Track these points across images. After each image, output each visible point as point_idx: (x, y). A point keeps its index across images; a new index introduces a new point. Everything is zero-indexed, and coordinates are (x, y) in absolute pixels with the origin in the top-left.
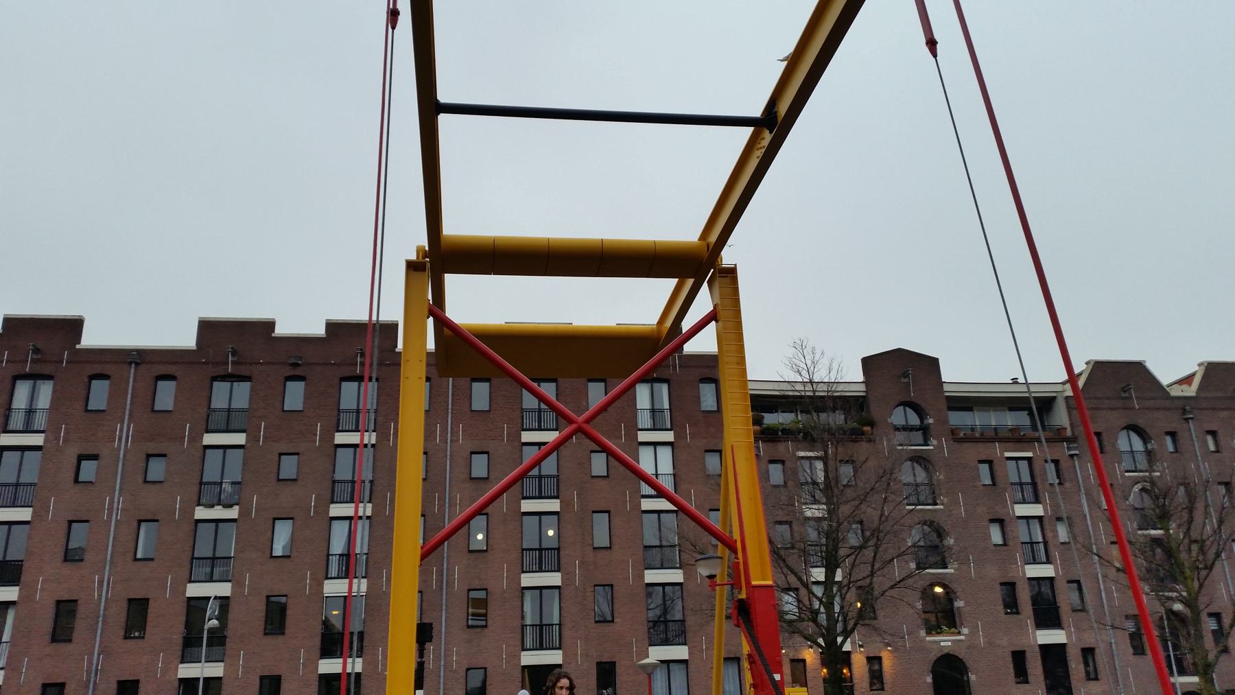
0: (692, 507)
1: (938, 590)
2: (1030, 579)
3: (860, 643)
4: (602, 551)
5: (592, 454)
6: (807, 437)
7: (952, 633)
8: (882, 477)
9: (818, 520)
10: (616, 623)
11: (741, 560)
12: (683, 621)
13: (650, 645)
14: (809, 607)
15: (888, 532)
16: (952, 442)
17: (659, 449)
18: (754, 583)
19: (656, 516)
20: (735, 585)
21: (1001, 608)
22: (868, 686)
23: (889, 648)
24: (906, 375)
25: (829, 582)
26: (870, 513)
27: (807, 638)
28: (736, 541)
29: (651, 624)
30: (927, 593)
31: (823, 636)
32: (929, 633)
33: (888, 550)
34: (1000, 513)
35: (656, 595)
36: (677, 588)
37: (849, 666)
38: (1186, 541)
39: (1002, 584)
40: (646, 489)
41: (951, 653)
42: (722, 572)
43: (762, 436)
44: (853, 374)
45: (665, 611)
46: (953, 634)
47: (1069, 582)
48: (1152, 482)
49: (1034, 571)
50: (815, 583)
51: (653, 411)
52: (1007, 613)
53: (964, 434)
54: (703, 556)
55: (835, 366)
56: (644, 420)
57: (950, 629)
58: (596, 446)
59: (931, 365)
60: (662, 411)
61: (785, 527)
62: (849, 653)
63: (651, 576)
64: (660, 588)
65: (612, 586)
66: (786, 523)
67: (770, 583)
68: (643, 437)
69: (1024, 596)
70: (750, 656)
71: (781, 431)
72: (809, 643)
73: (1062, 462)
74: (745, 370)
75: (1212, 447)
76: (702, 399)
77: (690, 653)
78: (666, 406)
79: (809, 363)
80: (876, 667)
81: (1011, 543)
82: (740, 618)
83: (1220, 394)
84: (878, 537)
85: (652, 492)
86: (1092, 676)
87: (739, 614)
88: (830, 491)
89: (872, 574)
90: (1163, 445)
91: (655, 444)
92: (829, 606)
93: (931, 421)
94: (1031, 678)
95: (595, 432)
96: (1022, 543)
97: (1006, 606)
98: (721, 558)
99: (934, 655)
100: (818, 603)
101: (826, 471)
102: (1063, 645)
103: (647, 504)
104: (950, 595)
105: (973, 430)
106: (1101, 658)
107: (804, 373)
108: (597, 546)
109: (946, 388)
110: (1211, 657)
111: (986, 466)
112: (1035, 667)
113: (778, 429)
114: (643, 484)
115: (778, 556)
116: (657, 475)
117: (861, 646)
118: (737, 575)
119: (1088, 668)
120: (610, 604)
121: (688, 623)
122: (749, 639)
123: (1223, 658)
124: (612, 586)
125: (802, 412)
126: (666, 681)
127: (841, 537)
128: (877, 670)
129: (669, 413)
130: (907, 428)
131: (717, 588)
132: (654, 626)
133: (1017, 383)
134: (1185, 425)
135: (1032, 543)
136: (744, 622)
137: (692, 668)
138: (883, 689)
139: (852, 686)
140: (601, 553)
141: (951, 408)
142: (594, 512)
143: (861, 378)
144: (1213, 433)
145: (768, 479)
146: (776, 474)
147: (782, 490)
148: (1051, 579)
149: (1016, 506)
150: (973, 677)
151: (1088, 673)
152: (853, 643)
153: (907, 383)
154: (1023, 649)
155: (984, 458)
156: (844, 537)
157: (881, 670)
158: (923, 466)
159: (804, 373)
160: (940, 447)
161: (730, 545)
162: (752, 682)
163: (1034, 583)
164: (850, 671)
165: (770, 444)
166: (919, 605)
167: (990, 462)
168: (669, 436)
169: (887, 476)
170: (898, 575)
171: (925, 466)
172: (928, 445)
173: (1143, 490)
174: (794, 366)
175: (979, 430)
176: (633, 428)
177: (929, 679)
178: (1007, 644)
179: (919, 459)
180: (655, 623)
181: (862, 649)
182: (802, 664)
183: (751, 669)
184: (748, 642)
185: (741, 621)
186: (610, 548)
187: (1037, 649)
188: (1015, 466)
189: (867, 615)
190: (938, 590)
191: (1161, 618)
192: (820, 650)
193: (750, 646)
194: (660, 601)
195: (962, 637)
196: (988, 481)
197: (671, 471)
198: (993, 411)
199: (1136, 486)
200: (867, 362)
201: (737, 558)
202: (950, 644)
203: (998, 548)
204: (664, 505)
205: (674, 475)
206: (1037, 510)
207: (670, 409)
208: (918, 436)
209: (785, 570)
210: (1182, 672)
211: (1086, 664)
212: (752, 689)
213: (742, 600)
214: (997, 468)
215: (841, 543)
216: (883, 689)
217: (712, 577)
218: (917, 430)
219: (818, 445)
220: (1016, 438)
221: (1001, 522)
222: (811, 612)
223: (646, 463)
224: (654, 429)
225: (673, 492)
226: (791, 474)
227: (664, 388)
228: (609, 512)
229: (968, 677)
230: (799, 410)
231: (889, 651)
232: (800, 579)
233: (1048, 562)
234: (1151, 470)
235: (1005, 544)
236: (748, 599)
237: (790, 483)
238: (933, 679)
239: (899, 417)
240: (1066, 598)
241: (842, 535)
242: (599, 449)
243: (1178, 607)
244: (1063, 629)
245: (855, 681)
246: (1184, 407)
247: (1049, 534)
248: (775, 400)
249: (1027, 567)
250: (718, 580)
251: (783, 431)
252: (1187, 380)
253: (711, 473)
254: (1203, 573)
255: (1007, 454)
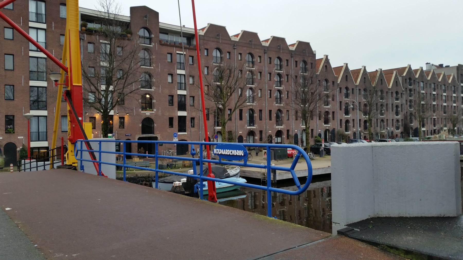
0: (53, 56)
1: (148, 96)
2: (178, 95)
3: (117, 112)
4: (10, 71)
5: (5, 28)
6: (105, 35)
7: (150, 110)
8: (132, 53)
9: (106, 67)
10: (15, 100)
11: (69, 76)
12: (46, 102)
13: (30, 110)
14: (98, 97)
15: (131, 73)
16: (159, 45)
17: (39, 31)
18: (74, 84)
19: (36, 59)
20: (66, 84)
21: (168, 103)
22: (119, 127)
23: (128, 115)
24: (146, 17)
25: (107, 91)
26: (126, 66)
27: (96, 109)
28: (68, 68)
29: (32, 102)
30: (144, 97)
31: (103, 109)
32: (142, 110)
33: (130, 80)
34: (172, 72)
35: (35, 92)
36: (45, 89)
37: (112, 120)
38: (226, 86)
39: (169, 96)
40: (32, 47)
41: (149, 117)
42: (62, 79)
43: (86, 32)
44: (125, 13)
45: (38, 97)
46: (151, 111)
47: (190, 97)
48: (220, 67)
49: (180, 92)
50: (102, 90)
51: (37, 14)
52: (169, 105)
53: (164, 43)
54: (53, 73)
55: (118, 7)
56: (32, 17)
57: (150, 109)
58: (9, 25)
59: (156, 14)
60: (42, 14)
61: (93, 69)
62: (112, 116)
63: (32, 83)
64: (36, 88)
65: (13, 86)
66: (93, 67)
67: (81, 85)
68: (31, 24)
69: (176, 100)
70: (70, 111)
71: (94, 31)
72: (98, 111)
73: (194, 57)
74: (78, 4)
75: (240, 59)
76: (61, 12)
77: (48, 113)
78: (43, 12)
79: (108, 4)
80: (122, 121)
81: (174, 82)
82: (67, 97)
83: (245, 42)
84: (127, 74)
85: (35, 48)
86: (193, 126)
87: (66, 95)
88: (111, 56)
89: (123, 88)
90: (226, 56)
91: (37, 29)
92: (106, 98)
93: (153, 36)
94: (174, 126)
95: (4, 15)
96: (178, 83)
97: (169, 103)
98: (61, 74)
99: (143, 118)
100: (102, 96)
101: (110, 49)
102: (185, 116)
103: (31, 54)
104: (151, 99)
105: (167, 41)
106: (196, 121)
107: (106, 8)
108: (7, 69)
109: (160, 24)
110: (226, 121)
111: (170, 55)
112: (176, 123)
113: (93, 30)
114: (30, 44)
115: (85, 75)
116: (37, 42)
117: (118, 113)
118: (67, 81)
119: (192, 124)
120: (13, 93)
121: (48, 102)
122: (70, 104)
123: (229, 121)
124: (13, 86)
125: (104, 24)
126: (37, 126)
127: (114, 74)
128: (122, 122)
129: (45, 16)
130: (144, 38)
131: (59, 85)
132: (33, 103)
133: (184, 27)
134: (233, 50)
135: (181, 83)
136: (68, 98)
137: (48, 119)
138: (124, 128)
139: (113, 127)
140: (8, 73)
141: (160, 33)
142: (5, 54)
143: (129, 15)
144: (241, 54)
145: (87, 49)
146: (91, 48)
147: (92, 54)
148: (185, 95)
149: (178, 70)
150: (155, 125)
151: (192, 125)
152: (115, 112)
153: (146, 20)
154: (172, 117)
155: (191, 55)
156: (114, 74)
157: (124, 122)
158: (147, 51)
159: (106, 8)
160: (155, 46)
161: (65, 70)
162: (70, 120)
163: (180, 96)
164: (112, 122)
165: (89, 35)
166: (140, 101)
167: (171, 54)
168: (44, 26)
169: (134, 53)
170: (134, 88)
171: (148, 51)
172: (151, 45)
173: (217, 70)
174: (102, 4)
175: (169, 42)
176: (27, 20)
177: (141, 125)
178: (168, 115)
179: (146, 49)
180: (34, 102)
181: (118, 115)
182: (94, 119)
183: (70, 116)
184: (69, 106)
185: (67, 98)
186: (13, 70)
187: (177, 117)
188: (27, 164)
189: (121, 102)
190: (148, 96)
191: (215, 110)
192: (102, 114)
193: (70, 107)
194: (36, 94)
195: (154, 112)
196: (170, 60)
197: (44, 41)
198: (175, 36)
199: (216, 68)
200: (133, 10)
201: (68, 75)
202: (149, 114)
203: (169, 83)
204: (42, 55)
205: (46, 43)
206: (183, 72)
207: (45, 14)
208: (148, 41)
209: (90, 83)
210: (218, 126)
211: (191, 123)
212: (70, 123)
213: (68, 91)
214: (173, 55)
215: (113, 76)
216: (124, 128)
217: (56, 81)
218: (147, 38)
219: (109, 39)
220: (179, 46)
221: (172, 75)
222: (99, 99)
223: (32, 34)
224: (37, 22)
225: (45, 49)
226: (97, 50)
227: (43, 4)
228: (13, 55)
229: (154, 125)
230: (102, 24)
231: (128, 115)
232: (95, 87)
233: (185, 90)
234: (221, 63)
235: (172, 83)
236: (70, 90)
237: (96, 52)
238: (142, 125)
239: (142, 32)
240: (189, 102)
241: (114, 73)
242: (11, 27)
243: (221, 106)
244: (186, 111)
245: (114, 125)
246: (234, 44)
247: (187, 81)
248: (94, 18)
249: (178, 91)
250: (59, 82)
251: (95, 31)
252: (237, 36)
253: (62, 44)
254: (228, 97)
255: (177, 52)
